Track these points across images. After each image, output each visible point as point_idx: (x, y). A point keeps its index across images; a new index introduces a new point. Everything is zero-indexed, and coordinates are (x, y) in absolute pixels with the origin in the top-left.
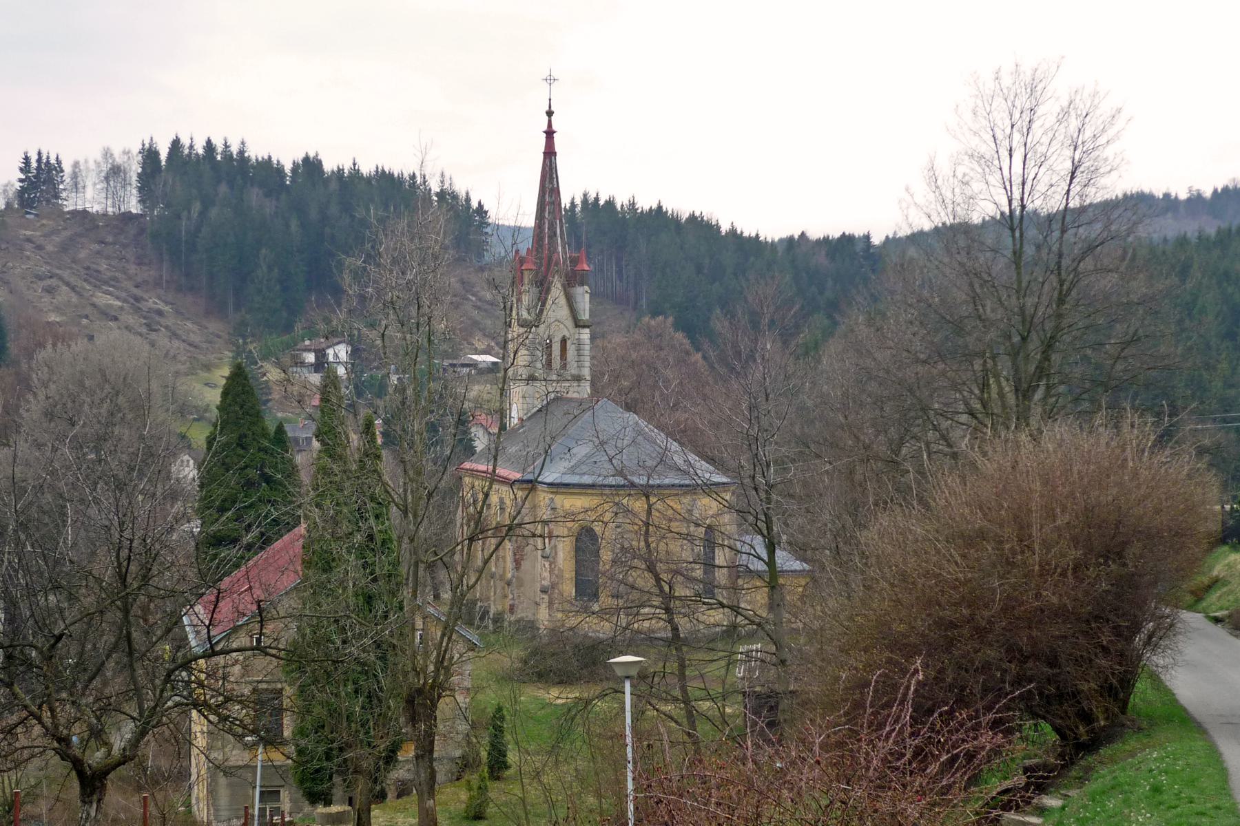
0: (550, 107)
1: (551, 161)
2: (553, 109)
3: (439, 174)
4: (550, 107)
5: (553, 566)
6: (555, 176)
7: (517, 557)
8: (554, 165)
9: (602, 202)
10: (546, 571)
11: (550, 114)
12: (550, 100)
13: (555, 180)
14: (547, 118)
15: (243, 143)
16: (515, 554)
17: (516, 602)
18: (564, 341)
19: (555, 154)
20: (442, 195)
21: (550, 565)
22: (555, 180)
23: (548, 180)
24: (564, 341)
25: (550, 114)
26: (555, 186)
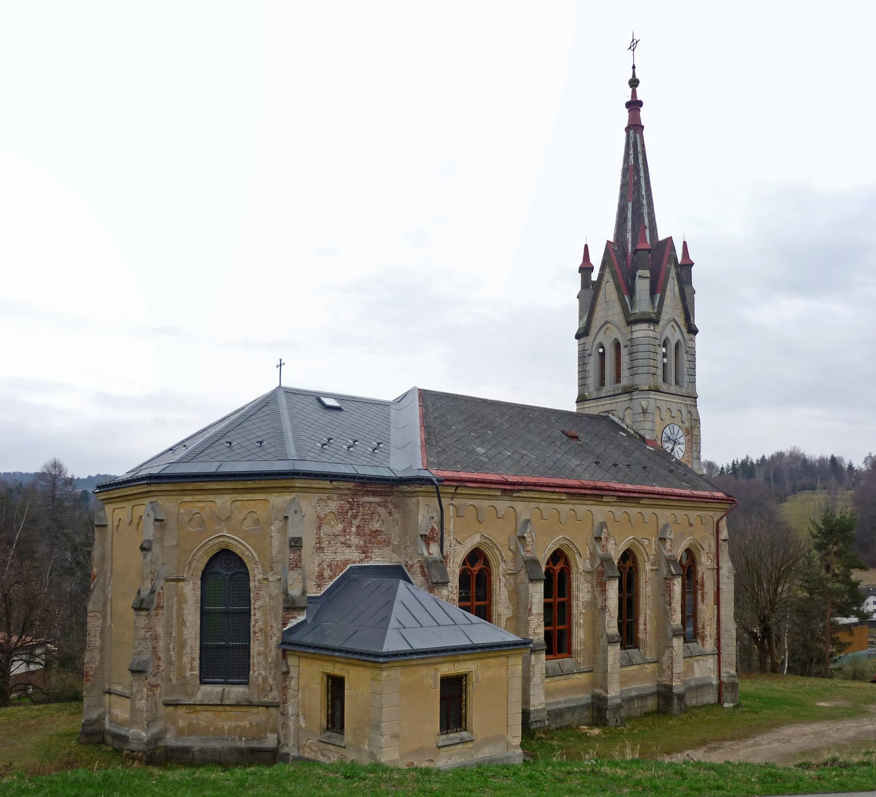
0: (634, 75)
4: (634, 75)
11: (634, 83)
12: (634, 67)
24: (617, 345)
25: (634, 83)
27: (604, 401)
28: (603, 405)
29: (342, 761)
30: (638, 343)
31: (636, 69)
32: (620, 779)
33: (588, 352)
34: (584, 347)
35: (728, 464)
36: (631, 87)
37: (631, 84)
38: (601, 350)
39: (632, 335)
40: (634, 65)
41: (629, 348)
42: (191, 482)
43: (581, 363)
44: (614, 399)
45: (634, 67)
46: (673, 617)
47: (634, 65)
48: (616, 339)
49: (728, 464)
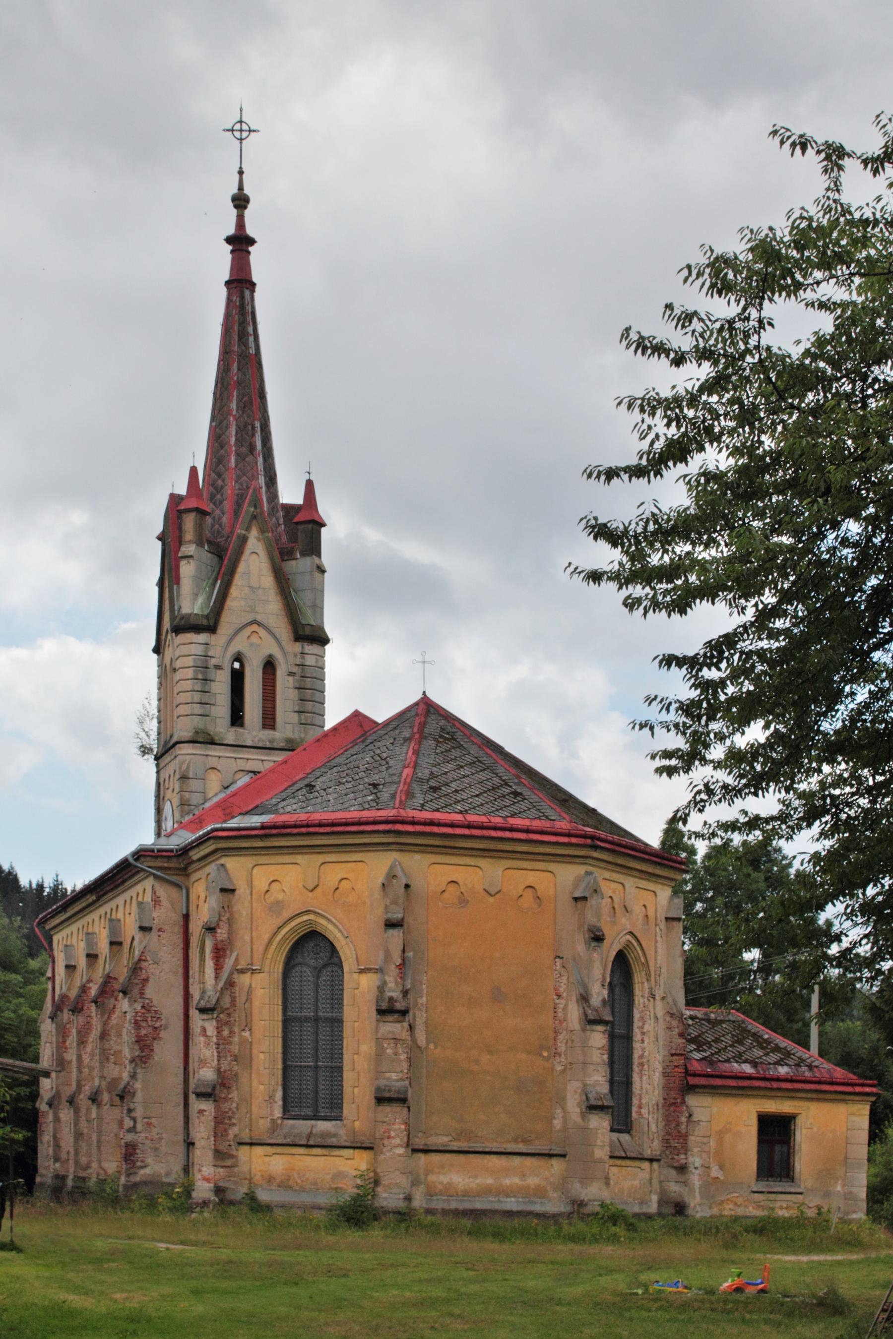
0: (241, 188)
1: (242, 297)
2: (247, 191)
3: (15, 1218)
4: (241, 188)
5: (226, 1033)
6: (250, 330)
7: (143, 1032)
8: (249, 308)
9: (689, 609)
10: (207, 1044)
11: (241, 201)
12: (241, 173)
13: (251, 339)
14: (234, 212)
15: (792, 155)
16: (137, 1024)
17: (140, 1138)
18: (269, 666)
19: (252, 286)
20: (10, 873)
21: (219, 1030)
22: (251, 339)
23: (236, 337)
24: (269, 666)
25: (241, 201)
26: (252, 351)
27: (248, 752)
28: (248, 759)
29: (618, 1217)
30: (314, 675)
31: (244, 176)
32: (826, 264)
33: (213, 662)
34: (207, 650)
35: (803, 153)
36: (236, 207)
37: (236, 203)
38: (237, 665)
39: (303, 658)
40: (241, 168)
41: (297, 678)
42: (62, 922)
43: (200, 677)
44: (267, 755)
45: (241, 173)
46: (860, 531)
47: (241, 168)
48: (270, 656)
49: (803, 153)
